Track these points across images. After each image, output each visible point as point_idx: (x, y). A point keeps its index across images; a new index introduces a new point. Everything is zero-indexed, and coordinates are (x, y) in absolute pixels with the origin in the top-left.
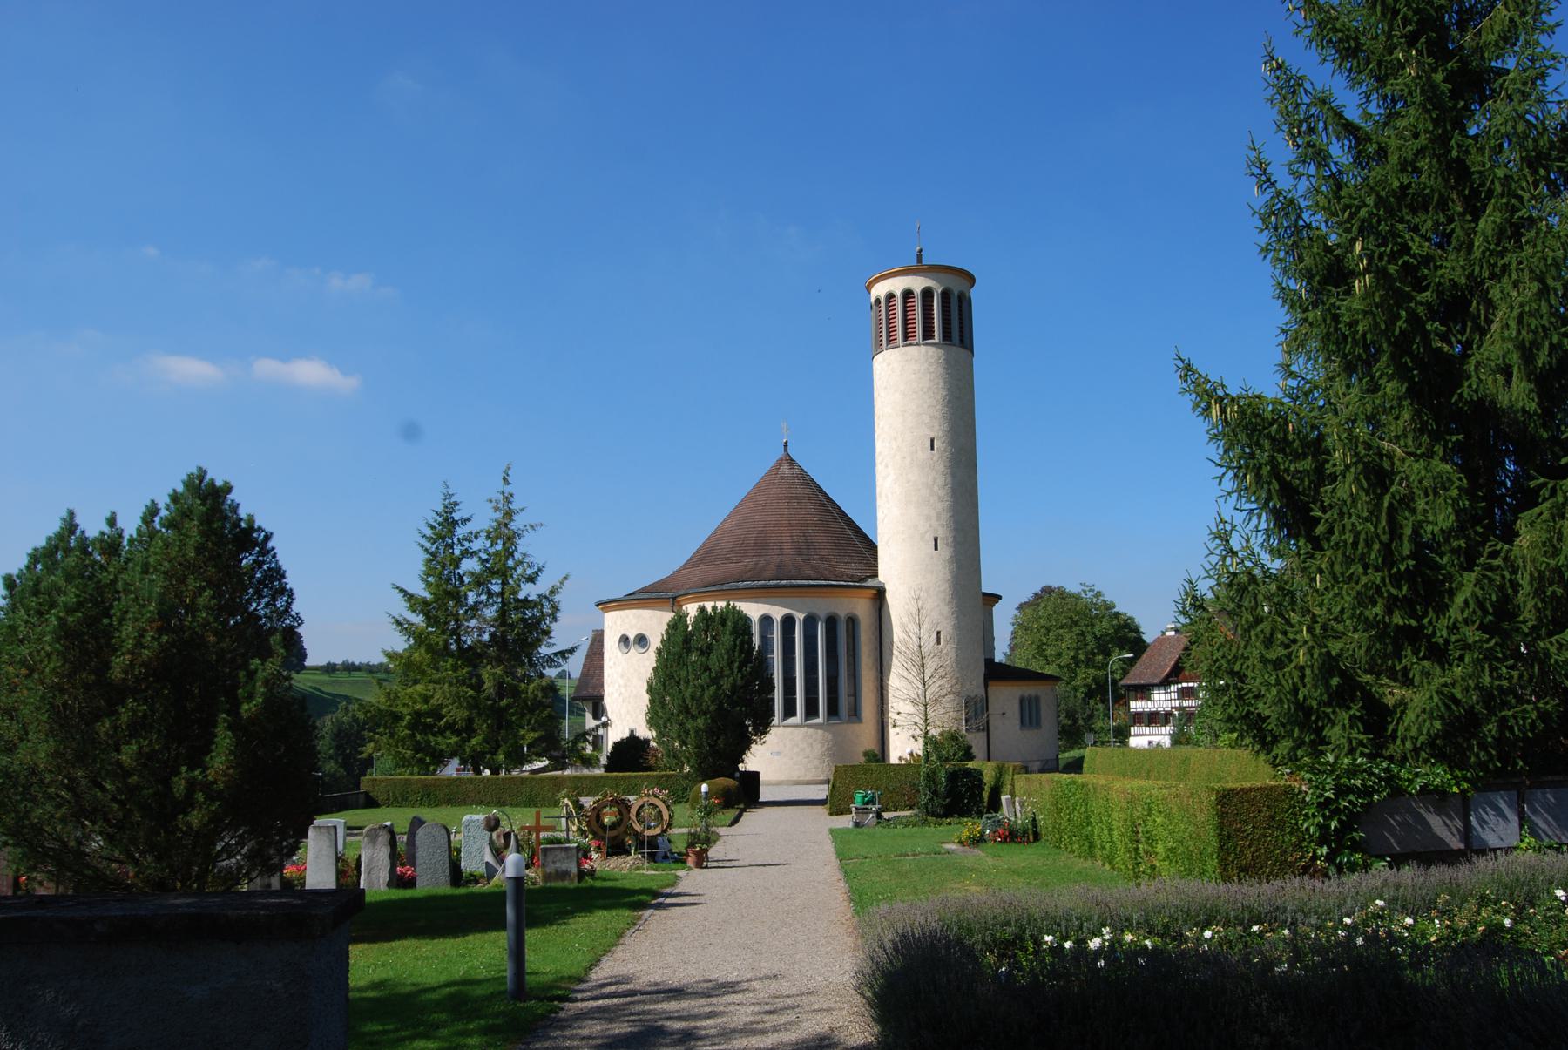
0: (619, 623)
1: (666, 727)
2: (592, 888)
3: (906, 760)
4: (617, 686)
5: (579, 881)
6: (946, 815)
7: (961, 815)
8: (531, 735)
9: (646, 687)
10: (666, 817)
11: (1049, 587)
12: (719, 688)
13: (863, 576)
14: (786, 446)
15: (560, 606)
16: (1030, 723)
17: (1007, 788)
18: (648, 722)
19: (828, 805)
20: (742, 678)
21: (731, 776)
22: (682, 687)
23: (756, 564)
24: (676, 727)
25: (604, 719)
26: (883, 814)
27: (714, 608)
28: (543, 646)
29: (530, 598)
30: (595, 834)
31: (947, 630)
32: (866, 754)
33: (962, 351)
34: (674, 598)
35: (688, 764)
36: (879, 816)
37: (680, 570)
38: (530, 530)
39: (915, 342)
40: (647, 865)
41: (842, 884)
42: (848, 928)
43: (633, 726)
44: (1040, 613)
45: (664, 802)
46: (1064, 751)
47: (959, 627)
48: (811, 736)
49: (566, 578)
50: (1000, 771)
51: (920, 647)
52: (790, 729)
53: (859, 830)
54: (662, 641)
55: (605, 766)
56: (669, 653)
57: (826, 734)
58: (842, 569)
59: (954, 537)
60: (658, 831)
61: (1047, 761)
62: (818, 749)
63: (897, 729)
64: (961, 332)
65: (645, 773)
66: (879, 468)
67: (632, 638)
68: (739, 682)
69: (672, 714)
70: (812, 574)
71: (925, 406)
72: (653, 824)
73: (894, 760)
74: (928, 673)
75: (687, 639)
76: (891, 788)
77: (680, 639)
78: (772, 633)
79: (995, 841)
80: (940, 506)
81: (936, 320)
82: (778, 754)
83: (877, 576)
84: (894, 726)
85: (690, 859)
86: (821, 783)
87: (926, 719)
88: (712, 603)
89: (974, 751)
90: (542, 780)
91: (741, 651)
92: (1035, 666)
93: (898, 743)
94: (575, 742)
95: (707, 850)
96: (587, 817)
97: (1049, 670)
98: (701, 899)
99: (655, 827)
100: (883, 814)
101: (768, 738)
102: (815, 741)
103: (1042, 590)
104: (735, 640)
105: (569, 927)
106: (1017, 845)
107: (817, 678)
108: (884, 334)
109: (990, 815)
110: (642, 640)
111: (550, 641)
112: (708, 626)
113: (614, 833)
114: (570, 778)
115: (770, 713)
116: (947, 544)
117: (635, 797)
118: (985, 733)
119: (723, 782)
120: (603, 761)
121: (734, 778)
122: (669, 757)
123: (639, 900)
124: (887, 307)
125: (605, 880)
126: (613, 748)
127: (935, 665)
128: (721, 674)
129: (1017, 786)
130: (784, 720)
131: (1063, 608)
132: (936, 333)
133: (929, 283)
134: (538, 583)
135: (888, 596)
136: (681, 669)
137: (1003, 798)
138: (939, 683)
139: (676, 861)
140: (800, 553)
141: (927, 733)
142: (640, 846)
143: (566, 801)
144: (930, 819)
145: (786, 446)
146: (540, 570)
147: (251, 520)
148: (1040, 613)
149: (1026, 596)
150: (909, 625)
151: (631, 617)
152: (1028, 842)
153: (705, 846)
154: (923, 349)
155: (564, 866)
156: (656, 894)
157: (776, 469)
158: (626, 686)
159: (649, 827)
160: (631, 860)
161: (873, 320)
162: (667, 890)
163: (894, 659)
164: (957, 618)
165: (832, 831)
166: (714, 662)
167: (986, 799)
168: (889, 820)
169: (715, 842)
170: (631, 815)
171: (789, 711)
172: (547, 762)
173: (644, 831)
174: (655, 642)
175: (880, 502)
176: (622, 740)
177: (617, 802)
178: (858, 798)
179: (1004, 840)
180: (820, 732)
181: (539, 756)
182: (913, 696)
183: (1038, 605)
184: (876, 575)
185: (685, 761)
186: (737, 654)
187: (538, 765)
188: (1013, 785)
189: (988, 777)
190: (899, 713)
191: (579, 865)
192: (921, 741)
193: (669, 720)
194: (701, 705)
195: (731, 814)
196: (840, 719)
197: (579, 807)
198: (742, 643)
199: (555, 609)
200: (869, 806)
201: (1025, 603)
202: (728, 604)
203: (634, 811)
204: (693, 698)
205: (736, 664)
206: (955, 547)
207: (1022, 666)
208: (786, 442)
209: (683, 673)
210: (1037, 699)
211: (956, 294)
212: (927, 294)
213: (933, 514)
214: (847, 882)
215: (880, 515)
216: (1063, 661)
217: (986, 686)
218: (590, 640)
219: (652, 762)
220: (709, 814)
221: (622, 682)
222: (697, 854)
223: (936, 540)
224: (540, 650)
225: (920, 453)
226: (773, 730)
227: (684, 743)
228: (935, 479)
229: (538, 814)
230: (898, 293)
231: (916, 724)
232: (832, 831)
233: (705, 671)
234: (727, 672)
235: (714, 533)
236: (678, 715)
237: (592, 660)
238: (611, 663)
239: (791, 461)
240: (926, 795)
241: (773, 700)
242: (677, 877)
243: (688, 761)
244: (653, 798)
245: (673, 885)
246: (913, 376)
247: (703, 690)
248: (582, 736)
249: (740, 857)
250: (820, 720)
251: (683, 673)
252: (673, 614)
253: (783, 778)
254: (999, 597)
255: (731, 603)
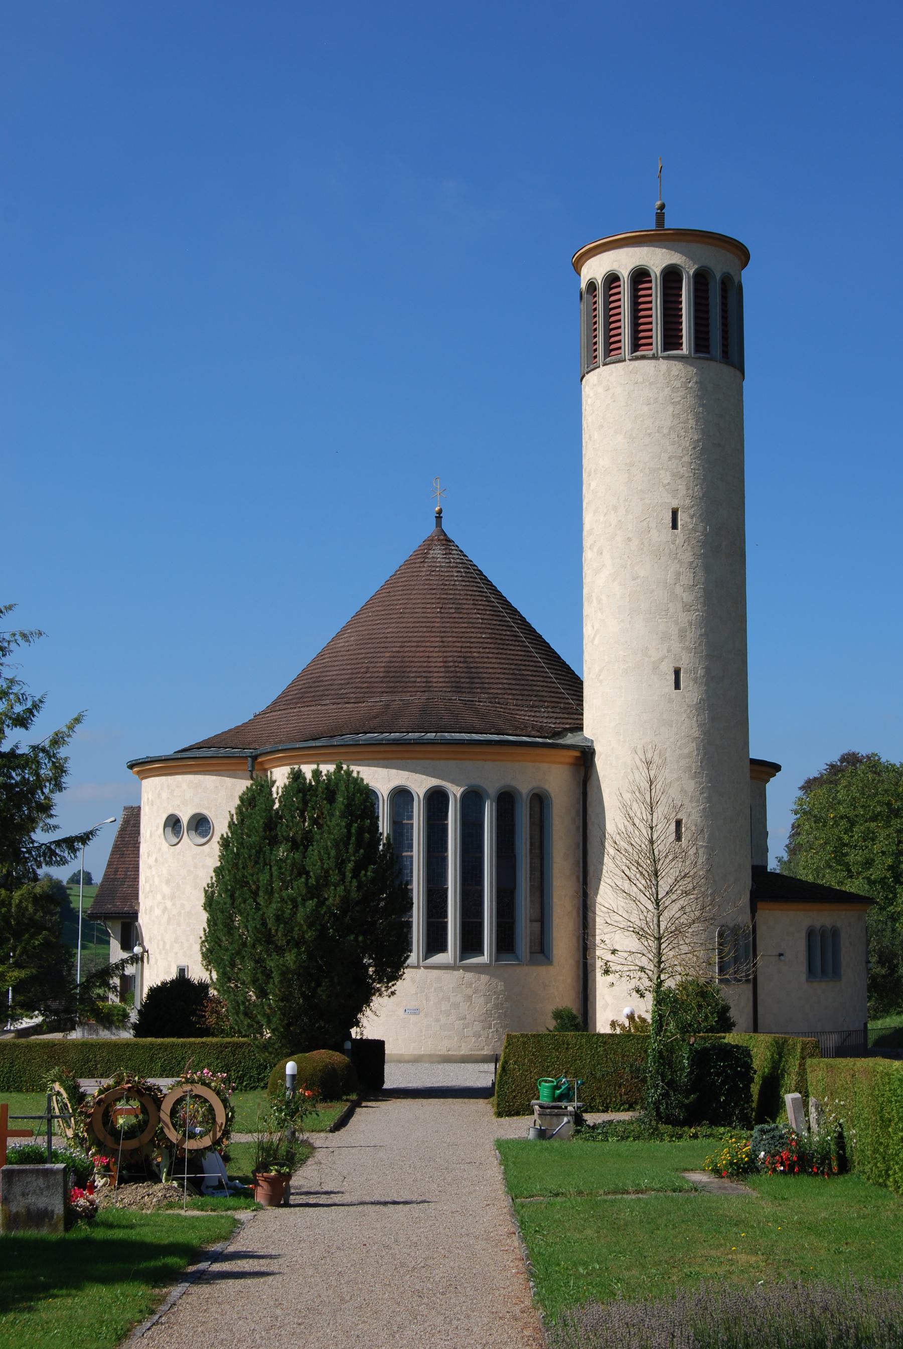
0: (164, 796)
1: (233, 965)
2: (87, 1242)
3: (623, 1027)
4: (159, 897)
5: (67, 1229)
6: (689, 1122)
7: (715, 1122)
8: (16, 974)
9: (202, 900)
10: (221, 1119)
11: (854, 755)
12: (321, 903)
13: (559, 727)
14: (439, 518)
15: (69, 766)
16: (823, 971)
17: (791, 1080)
18: (205, 956)
19: (494, 1099)
20: (359, 888)
21: (338, 1048)
22: (261, 900)
23: (387, 706)
24: (250, 965)
25: (137, 949)
26: (586, 1116)
27: (317, 774)
28: (38, 830)
29: (19, 752)
30: (100, 1145)
31: (692, 817)
32: (558, 1015)
33: (725, 368)
34: (254, 758)
35: (269, 1027)
36: (578, 1120)
37: (264, 713)
38: (20, 641)
39: (650, 353)
40: (186, 1199)
41: (515, 1241)
42: (526, 1326)
43: (183, 963)
44: (840, 796)
45: (218, 1093)
46: (875, 1018)
47: (711, 813)
48: (470, 985)
49: (78, 720)
50: (780, 1051)
51: (652, 842)
52: (436, 973)
53: (545, 1143)
54: (231, 825)
55: (135, 1027)
56: (241, 844)
57: (495, 981)
58: (524, 716)
59: (708, 669)
60: (207, 1141)
61: (849, 1034)
62: (480, 1005)
63: (610, 978)
64: (725, 338)
65: (199, 1040)
66: (588, 555)
67: (185, 820)
68: (354, 895)
69: (244, 944)
70: (476, 722)
71: (665, 456)
72: (198, 1130)
73: (602, 1026)
74: (664, 885)
75: (272, 822)
76: (599, 1075)
77: (259, 821)
78: (411, 817)
79: (774, 1170)
80: (684, 618)
81: (684, 319)
82: (416, 1012)
83: (581, 729)
84: (607, 972)
85: (259, 1189)
86: (485, 1060)
87: (660, 962)
88: (314, 767)
89: (733, 1014)
90: (30, 1047)
91: (359, 844)
92: (830, 879)
93: (609, 999)
94: (87, 986)
95: (288, 1176)
96: (89, 1116)
97: (854, 886)
98: (273, 1266)
99: (202, 1135)
100: (586, 1116)
101: (399, 986)
102: (476, 991)
103: (843, 759)
104: (349, 826)
105: (35, 1317)
106: (810, 1179)
107: (482, 891)
108: (600, 339)
109: (766, 1126)
110: (200, 824)
111: (49, 821)
112: (305, 802)
113: (132, 1144)
114: (75, 1045)
115: (405, 946)
116: (695, 680)
117: (170, 1081)
118: (751, 986)
119: (323, 1056)
120: (134, 1017)
121: (342, 1051)
122: (237, 1013)
123: (166, 1266)
124: (607, 296)
125: (110, 1226)
126: (149, 996)
127: (674, 873)
128: (324, 881)
129: (811, 1078)
130: (426, 958)
131: (876, 788)
132: (684, 340)
133: (675, 258)
134: (32, 728)
135: (600, 763)
136: (262, 871)
137: (789, 1098)
138: (681, 902)
139: (238, 1193)
140: (458, 689)
141: (660, 984)
142: (175, 1169)
143: (57, 1087)
144: (662, 1127)
145: (439, 518)
146: (36, 706)
147: (367, 784)
148: (840, 796)
149: (816, 767)
150: (635, 806)
151: (185, 786)
152: (830, 1173)
153: (285, 1170)
154: (663, 364)
155: (42, 1202)
156: (195, 1254)
157: (422, 554)
158: (173, 897)
159: (192, 1136)
160: (158, 1189)
161: (584, 318)
162: (217, 1247)
163: (606, 859)
164: (709, 799)
165: (501, 1145)
166: (314, 859)
167: (755, 1097)
168: (594, 1127)
169: (303, 1161)
170: (162, 1115)
171: (436, 943)
172: (40, 1019)
173: (182, 1141)
174: (221, 827)
175: (589, 610)
176: (164, 984)
177: (139, 1092)
178: (544, 1089)
179: (790, 1170)
180: (484, 978)
181: (29, 1008)
182: (638, 923)
183: (836, 783)
184: (579, 728)
185: (264, 1022)
186: (351, 848)
187: (26, 1023)
188: (802, 1073)
189: (760, 1060)
190: (614, 952)
191: (67, 1199)
192: (650, 997)
193: (238, 953)
194: (291, 930)
195: (334, 1110)
196: (517, 959)
197: (78, 1097)
198: (361, 831)
199: (60, 770)
200: (563, 1104)
201: (815, 779)
202: (339, 768)
203: (167, 1106)
204: (278, 919)
205: (350, 865)
206: (707, 684)
207: (810, 878)
208: (440, 512)
209: (264, 878)
210: (835, 933)
211: (718, 276)
212: (672, 275)
213: (674, 631)
214: (524, 1239)
215: (588, 630)
216: (875, 873)
217: (753, 910)
218: (120, 822)
219: (212, 1020)
220: (292, 1114)
221: (166, 890)
222: (271, 1181)
223: (677, 672)
224: (34, 836)
225: (654, 532)
226: (408, 974)
227: (262, 993)
228: (678, 574)
229: (11, 1118)
230: (625, 274)
231: (642, 969)
232: (501, 1145)
233: (300, 875)
234: (334, 877)
235: (321, 655)
236: (254, 946)
237: (122, 855)
238: (151, 861)
239: (447, 542)
240: (656, 1087)
241: (409, 925)
242: (236, 1223)
243: (269, 1022)
244: (199, 1086)
245: (228, 1237)
246: (646, 409)
247: (295, 906)
248: (103, 974)
249: (346, 1186)
250: (485, 959)
251: (264, 878)
252: (248, 783)
253: (422, 1051)
254: (776, 768)
255: (345, 767)
